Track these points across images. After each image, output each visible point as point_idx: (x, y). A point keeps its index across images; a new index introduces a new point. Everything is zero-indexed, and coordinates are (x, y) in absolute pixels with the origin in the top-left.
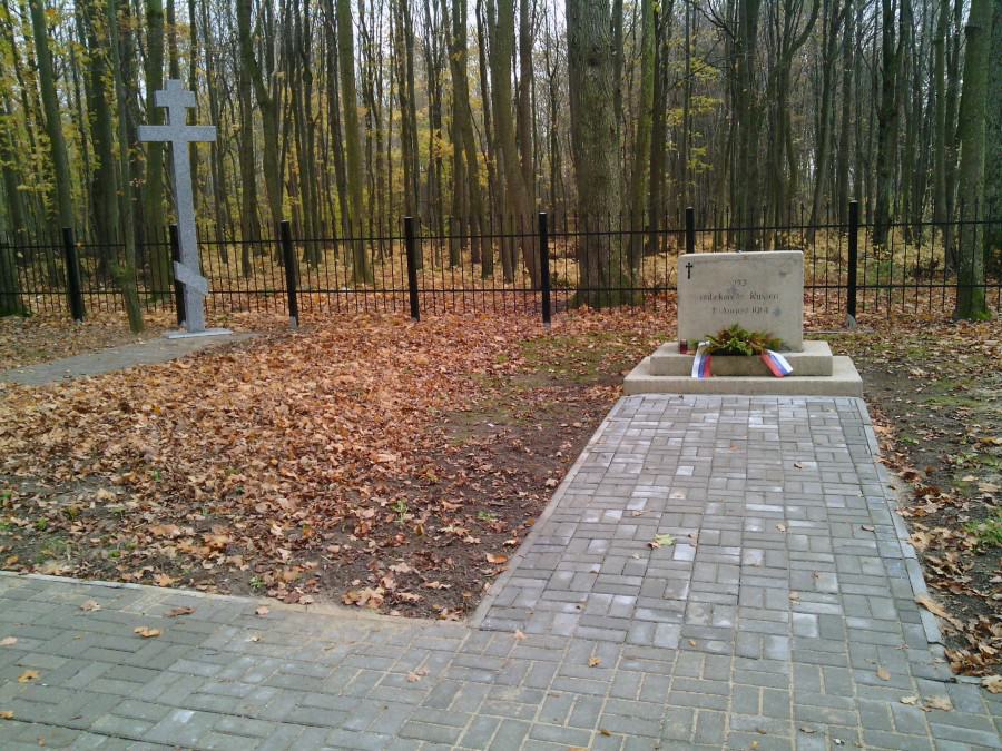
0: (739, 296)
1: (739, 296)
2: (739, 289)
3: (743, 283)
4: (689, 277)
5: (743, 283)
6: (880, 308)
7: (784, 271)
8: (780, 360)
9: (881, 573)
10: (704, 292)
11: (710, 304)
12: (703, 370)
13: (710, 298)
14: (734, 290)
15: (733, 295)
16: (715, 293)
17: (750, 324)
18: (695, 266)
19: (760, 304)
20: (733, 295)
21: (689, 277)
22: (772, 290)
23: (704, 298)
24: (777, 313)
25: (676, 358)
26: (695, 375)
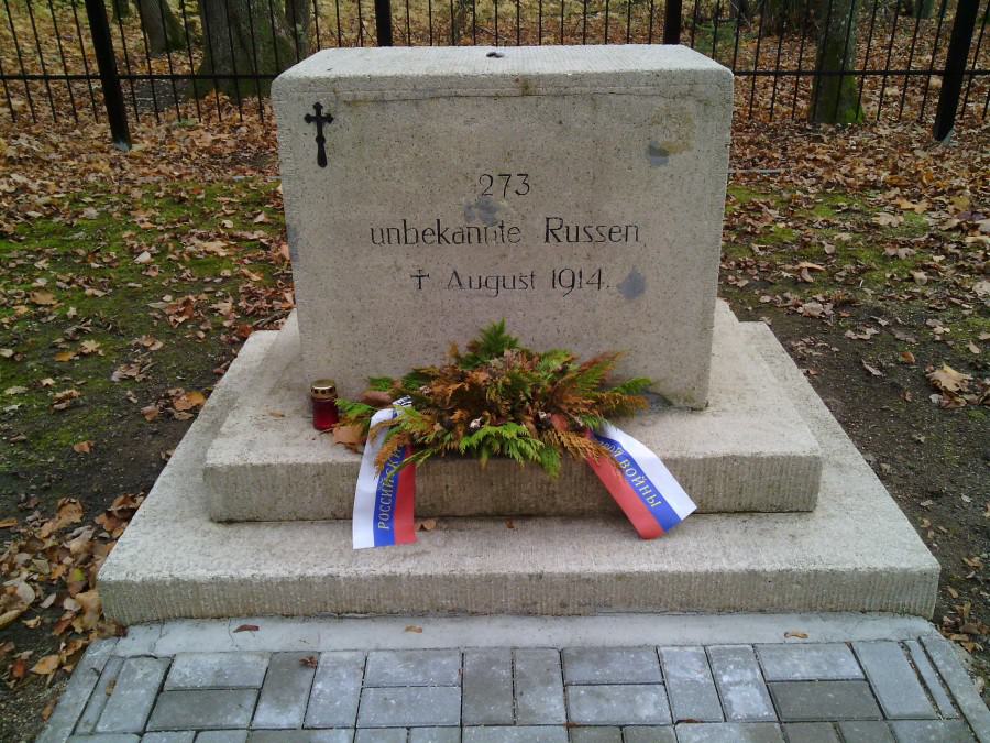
0: (506, 233)
1: (506, 233)
2: (505, 205)
3: (516, 182)
4: (322, 161)
5: (516, 182)
6: (897, 336)
7: (662, 140)
8: (641, 450)
9: (895, 724)
10: (383, 215)
11: (406, 259)
12: (388, 508)
13: (401, 234)
14: (488, 209)
15: (483, 227)
16: (421, 220)
17: (552, 328)
18: (341, 117)
19: (575, 258)
20: (483, 227)
21: (322, 161)
22: (616, 210)
23: (382, 236)
24: (634, 287)
25: (662, 81)
26: (363, 533)
